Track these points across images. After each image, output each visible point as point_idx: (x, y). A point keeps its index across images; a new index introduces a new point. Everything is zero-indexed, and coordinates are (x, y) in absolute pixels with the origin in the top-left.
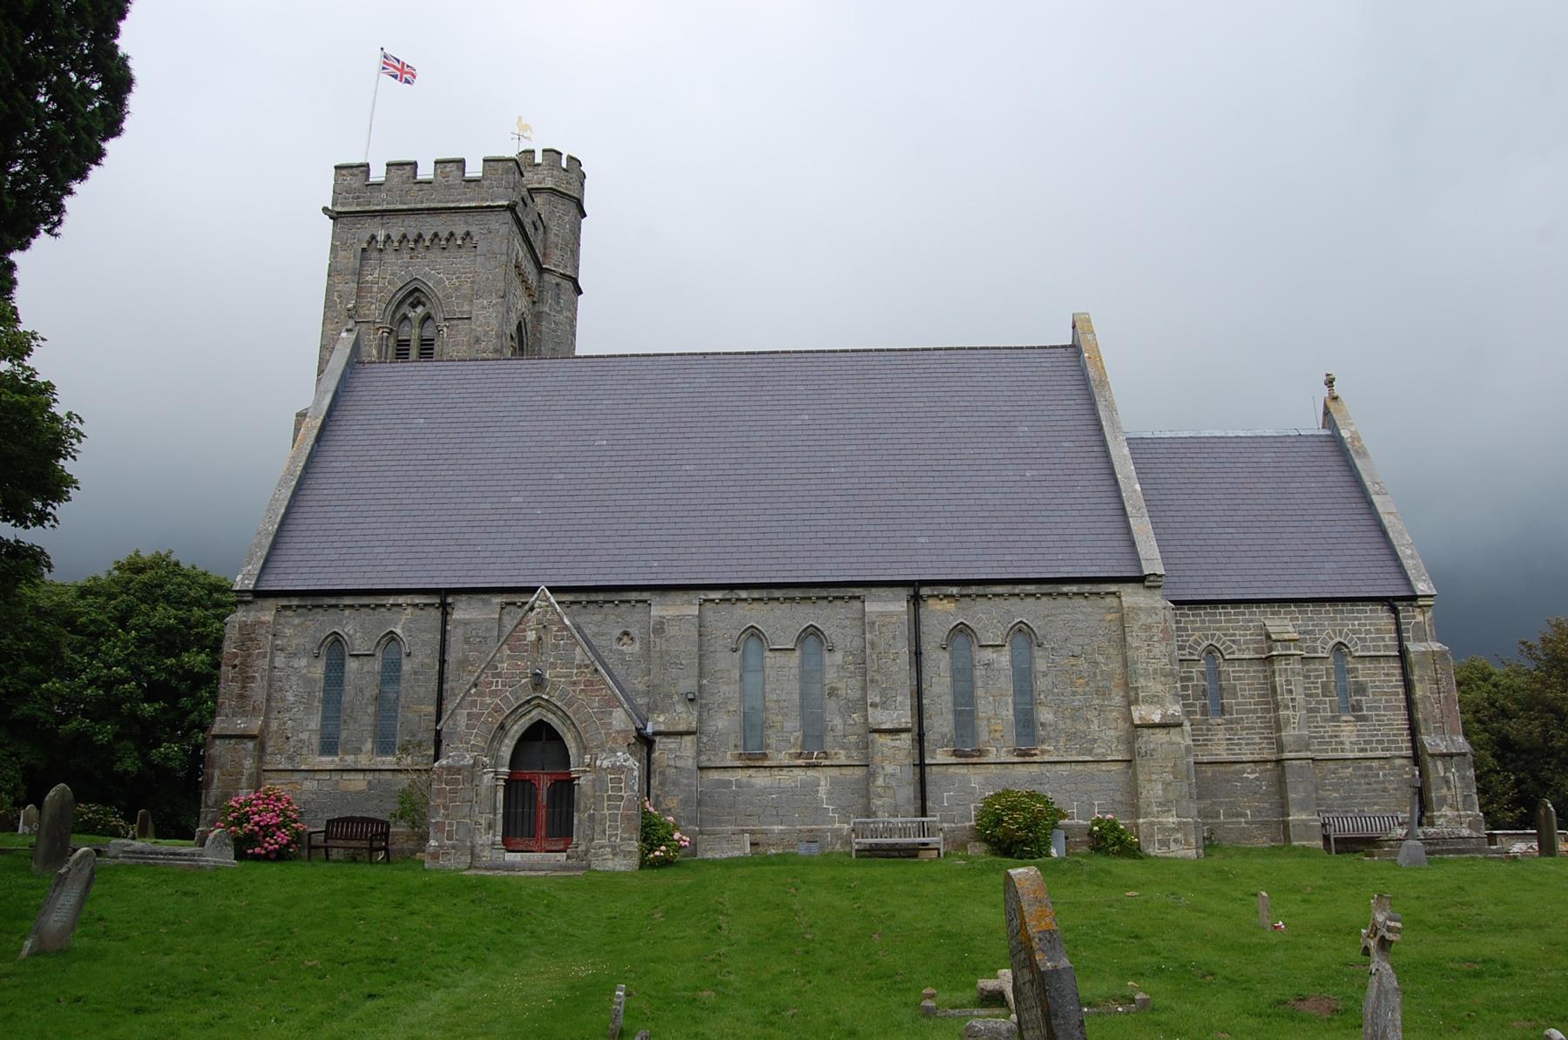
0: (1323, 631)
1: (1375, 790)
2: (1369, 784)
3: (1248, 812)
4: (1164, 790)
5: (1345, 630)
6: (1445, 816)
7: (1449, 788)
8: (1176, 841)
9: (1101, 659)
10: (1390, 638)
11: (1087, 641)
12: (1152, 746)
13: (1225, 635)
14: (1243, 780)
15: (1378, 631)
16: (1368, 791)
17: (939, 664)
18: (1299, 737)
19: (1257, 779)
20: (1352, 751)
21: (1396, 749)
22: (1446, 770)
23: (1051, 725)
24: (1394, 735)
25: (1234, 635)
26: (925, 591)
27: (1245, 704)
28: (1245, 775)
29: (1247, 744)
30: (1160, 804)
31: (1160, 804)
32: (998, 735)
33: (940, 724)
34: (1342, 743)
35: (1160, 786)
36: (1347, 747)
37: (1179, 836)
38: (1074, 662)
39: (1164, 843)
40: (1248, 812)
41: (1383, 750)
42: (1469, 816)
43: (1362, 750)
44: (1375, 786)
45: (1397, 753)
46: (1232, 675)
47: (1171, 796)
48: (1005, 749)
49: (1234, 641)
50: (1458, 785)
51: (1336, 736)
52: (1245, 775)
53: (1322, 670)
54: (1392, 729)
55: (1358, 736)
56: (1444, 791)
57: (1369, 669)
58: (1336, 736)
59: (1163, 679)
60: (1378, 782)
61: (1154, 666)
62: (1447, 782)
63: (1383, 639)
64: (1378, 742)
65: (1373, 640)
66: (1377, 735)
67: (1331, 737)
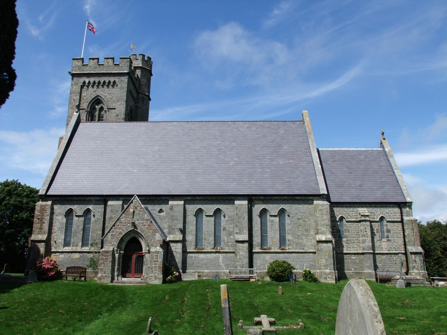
0: (377, 212)
1: (392, 263)
2: (391, 261)
3: (353, 269)
4: (326, 261)
5: (384, 212)
6: (415, 272)
7: (416, 263)
8: (329, 278)
9: (307, 220)
10: (398, 215)
11: (303, 214)
12: (322, 248)
13: (346, 213)
14: (351, 259)
15: (395, 213)
16: (390, 263)
17: (257, 220)
18: (368, 246)
19: (355, 259)
20: (386, 251)
21: (400, 250)
22: (415, 257)
23: (291, 240)
24: (399, 246)
25: (349, 213)
26: (253, 198)
27: (352, 235)
28: (352, 257)
29: (353, 248)
30: (324, 266)
31: (324, 266)
32: (275, 243)
33: (257, 239)
34: (382, 248)
35: (324, 260)
36: (384, 249)
37: (330, 276)
38: (299, 220)
39: (325, 278)
40: (353, 269)
41: (395, 250)
42: (422, 272)
43: (389, 250)
44: (392, 262)
45: (400, 252)
46: (348, 226)
47: (328, 263)
48: (277, 248)
49: (349, 215)
50: (419, 262)
51: (380, 246)
52: (352, 257)
53: (390, 227)
54: (398, 244)
55: (388, 246)
56: (415, 264)
57: (391, 225)
58: (380, 246)
59: (326, 227)
60: (393, 261)
61: (324, 223)
62: (415, 261)
63: (396, 216)
64: (394, 248)
65: (393, 216)
66: (393, 246)
67: (379, 246)
